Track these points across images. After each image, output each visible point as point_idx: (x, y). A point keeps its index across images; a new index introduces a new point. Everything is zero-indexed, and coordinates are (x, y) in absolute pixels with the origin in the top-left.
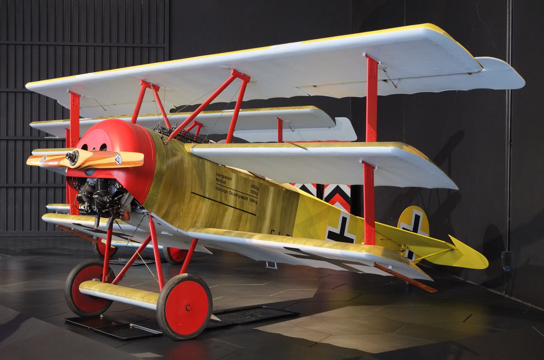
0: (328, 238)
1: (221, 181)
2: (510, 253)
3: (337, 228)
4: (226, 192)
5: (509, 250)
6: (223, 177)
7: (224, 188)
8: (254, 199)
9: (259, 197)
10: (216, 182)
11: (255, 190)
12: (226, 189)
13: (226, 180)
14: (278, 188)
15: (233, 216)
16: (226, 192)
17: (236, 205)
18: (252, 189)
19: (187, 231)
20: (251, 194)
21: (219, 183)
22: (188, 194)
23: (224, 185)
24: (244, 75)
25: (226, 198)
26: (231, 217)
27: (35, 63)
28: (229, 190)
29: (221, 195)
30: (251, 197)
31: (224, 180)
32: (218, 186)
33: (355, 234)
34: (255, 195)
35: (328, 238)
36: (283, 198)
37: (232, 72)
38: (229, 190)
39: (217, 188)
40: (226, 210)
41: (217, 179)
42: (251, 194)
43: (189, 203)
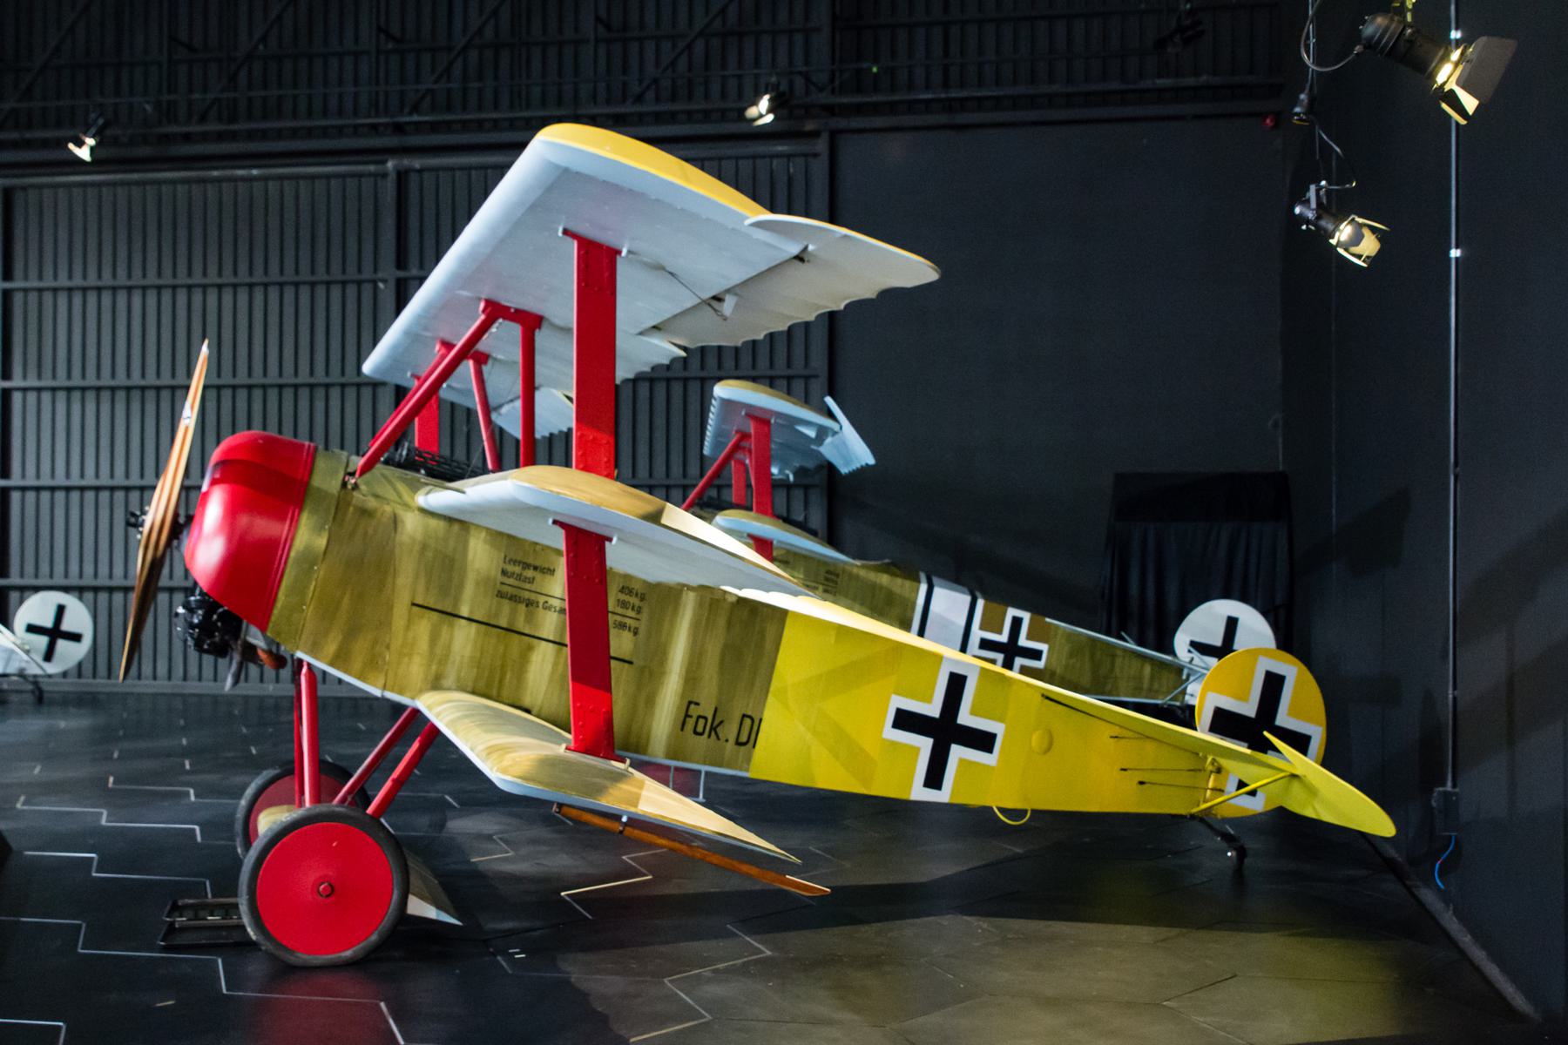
0: (994, 736)
1: (519, 577)
2: (1455, 794)
3: (928, 699)
4: (530, 603)
5: (1454, 786)
6: (526, 566)
7: (527, 595)
8: (628, 621)
9: (644, 616)
10: (500, 578)
11: (634, 600)
12: (533, 596)
13: (538, 575)
14: (711, 599)
15: (555, 664)
16: (530, 603)
17: (562, 635)
18: (623, 597)
19: (413, 698)
20: (620, 610)
21: (511, 581)
22: (401, 610)
23: (527, 586)
24: (517, 311)
25: (530, 618)
26: (548, 668)
27: (643, 418)
28: (542, 599)
29: (513, 612)
30: (619, 618)
31: (530, 573)
32: (505, 589)
33: (1001, 720)
34: (632, 614)
35: (994, 736)
36: (729, 623)
37: (482, 305)
38: (542, 599)
39: (500, 595)
40: (530, 648)
41: (504, 573)
42: (620, 610)
43: (408, 628)
